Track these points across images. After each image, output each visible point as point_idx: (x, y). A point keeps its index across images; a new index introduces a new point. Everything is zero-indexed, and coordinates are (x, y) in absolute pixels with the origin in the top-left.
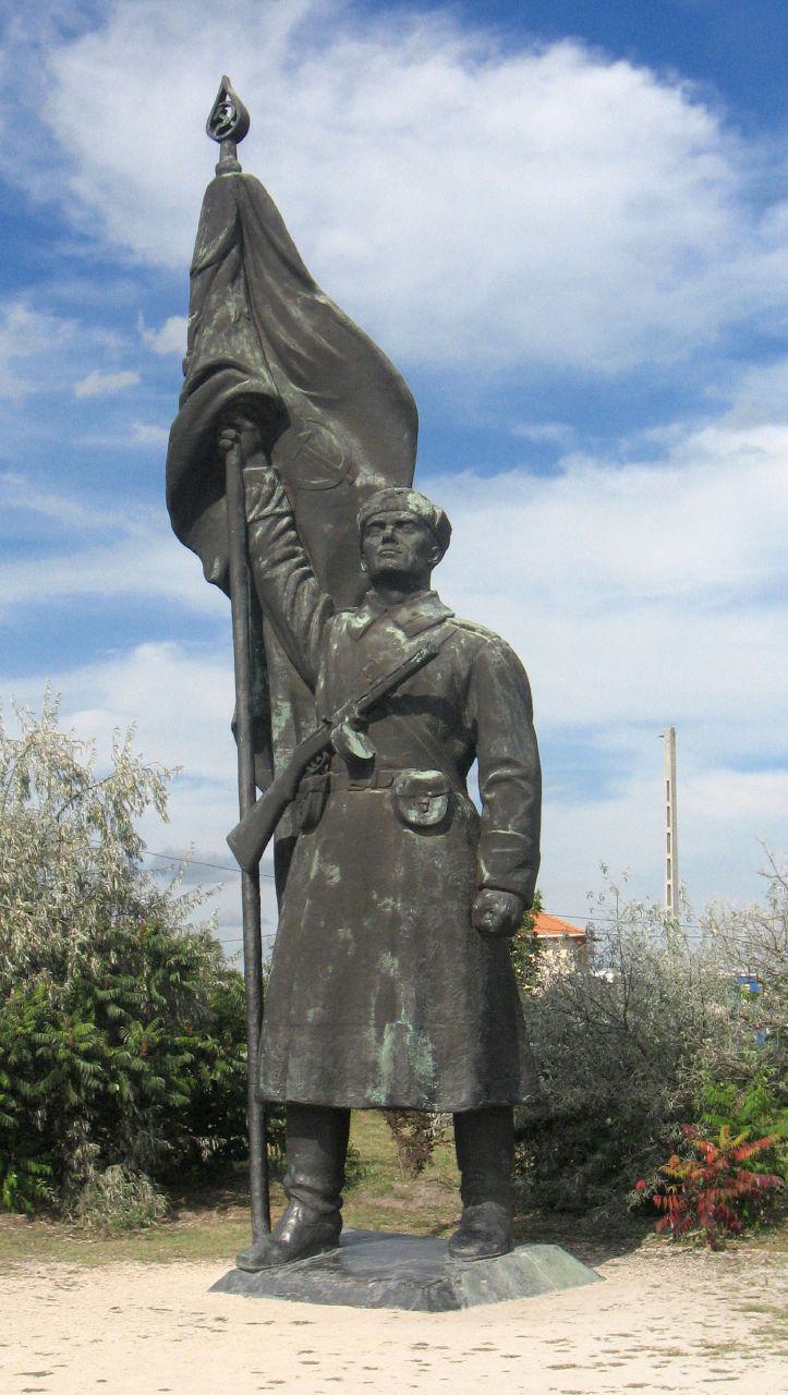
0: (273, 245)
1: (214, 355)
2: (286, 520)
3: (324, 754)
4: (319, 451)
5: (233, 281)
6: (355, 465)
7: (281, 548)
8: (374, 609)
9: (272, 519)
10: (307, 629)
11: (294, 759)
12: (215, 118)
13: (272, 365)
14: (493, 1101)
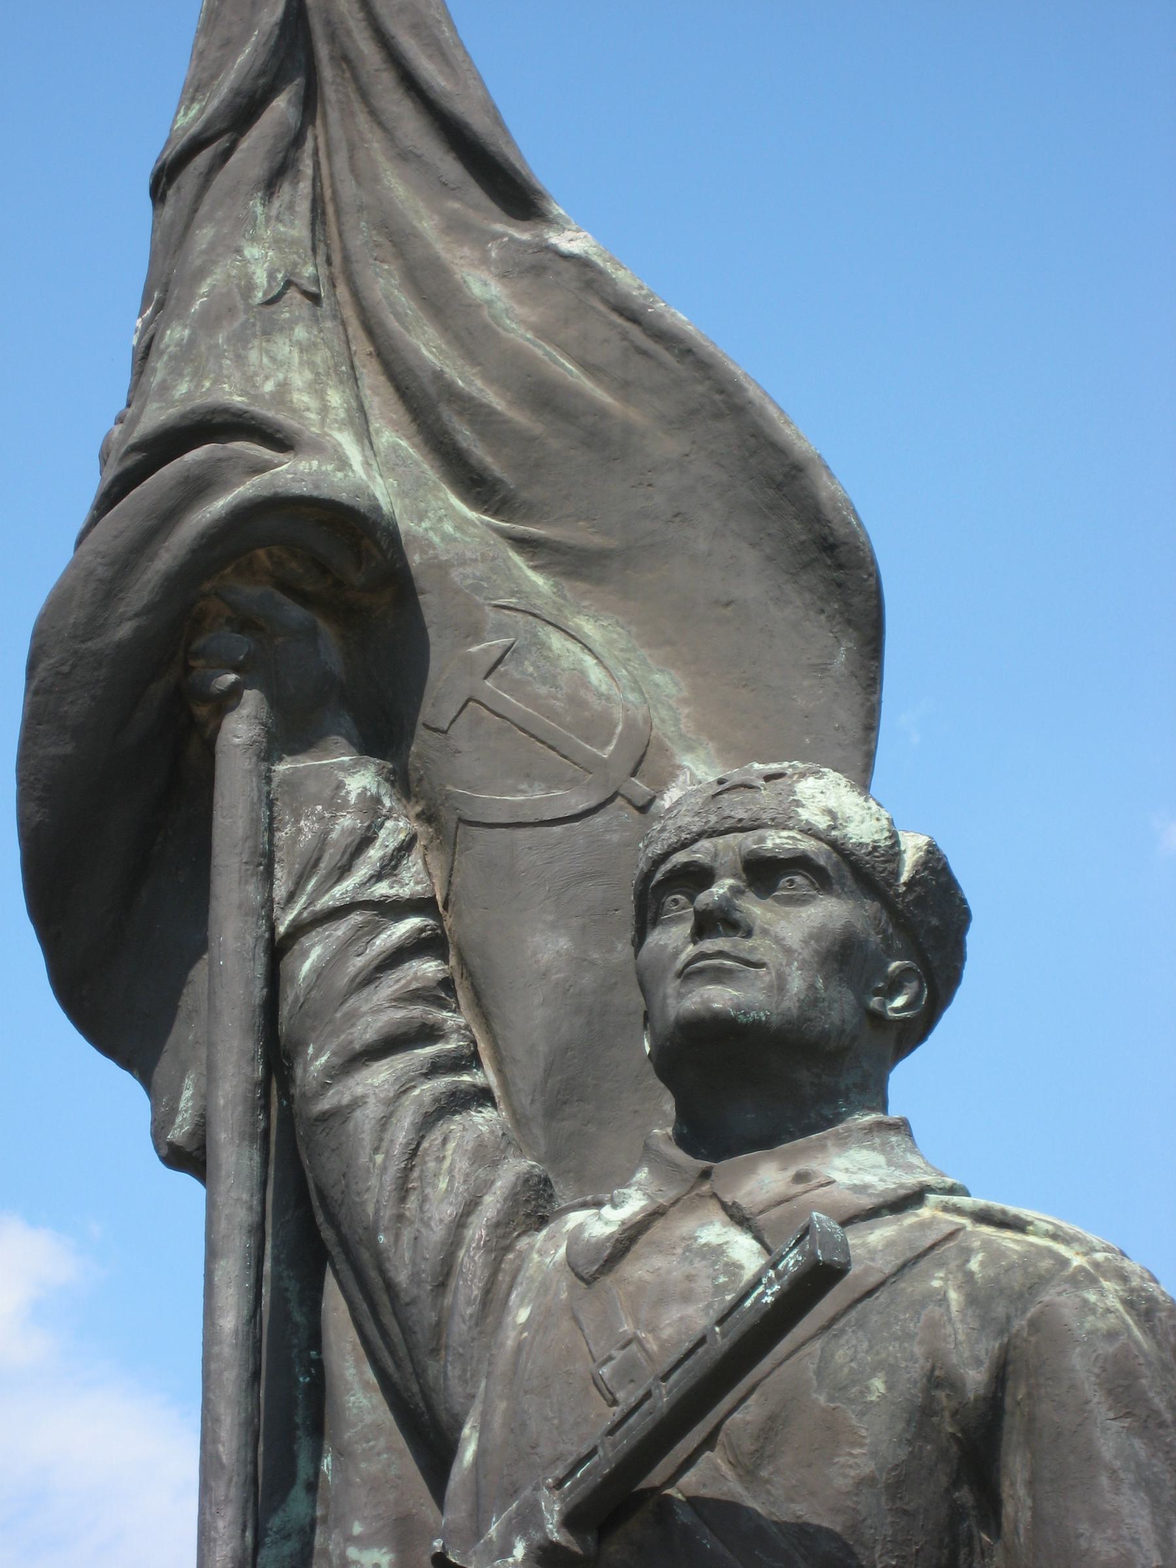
0: (410, 82)
1: (189, 395)
4: (533, 700)
6: (663, 750)
7: (377, 1010)
8: (664, 1169)
9: (356, 918)
13: (386, 437)
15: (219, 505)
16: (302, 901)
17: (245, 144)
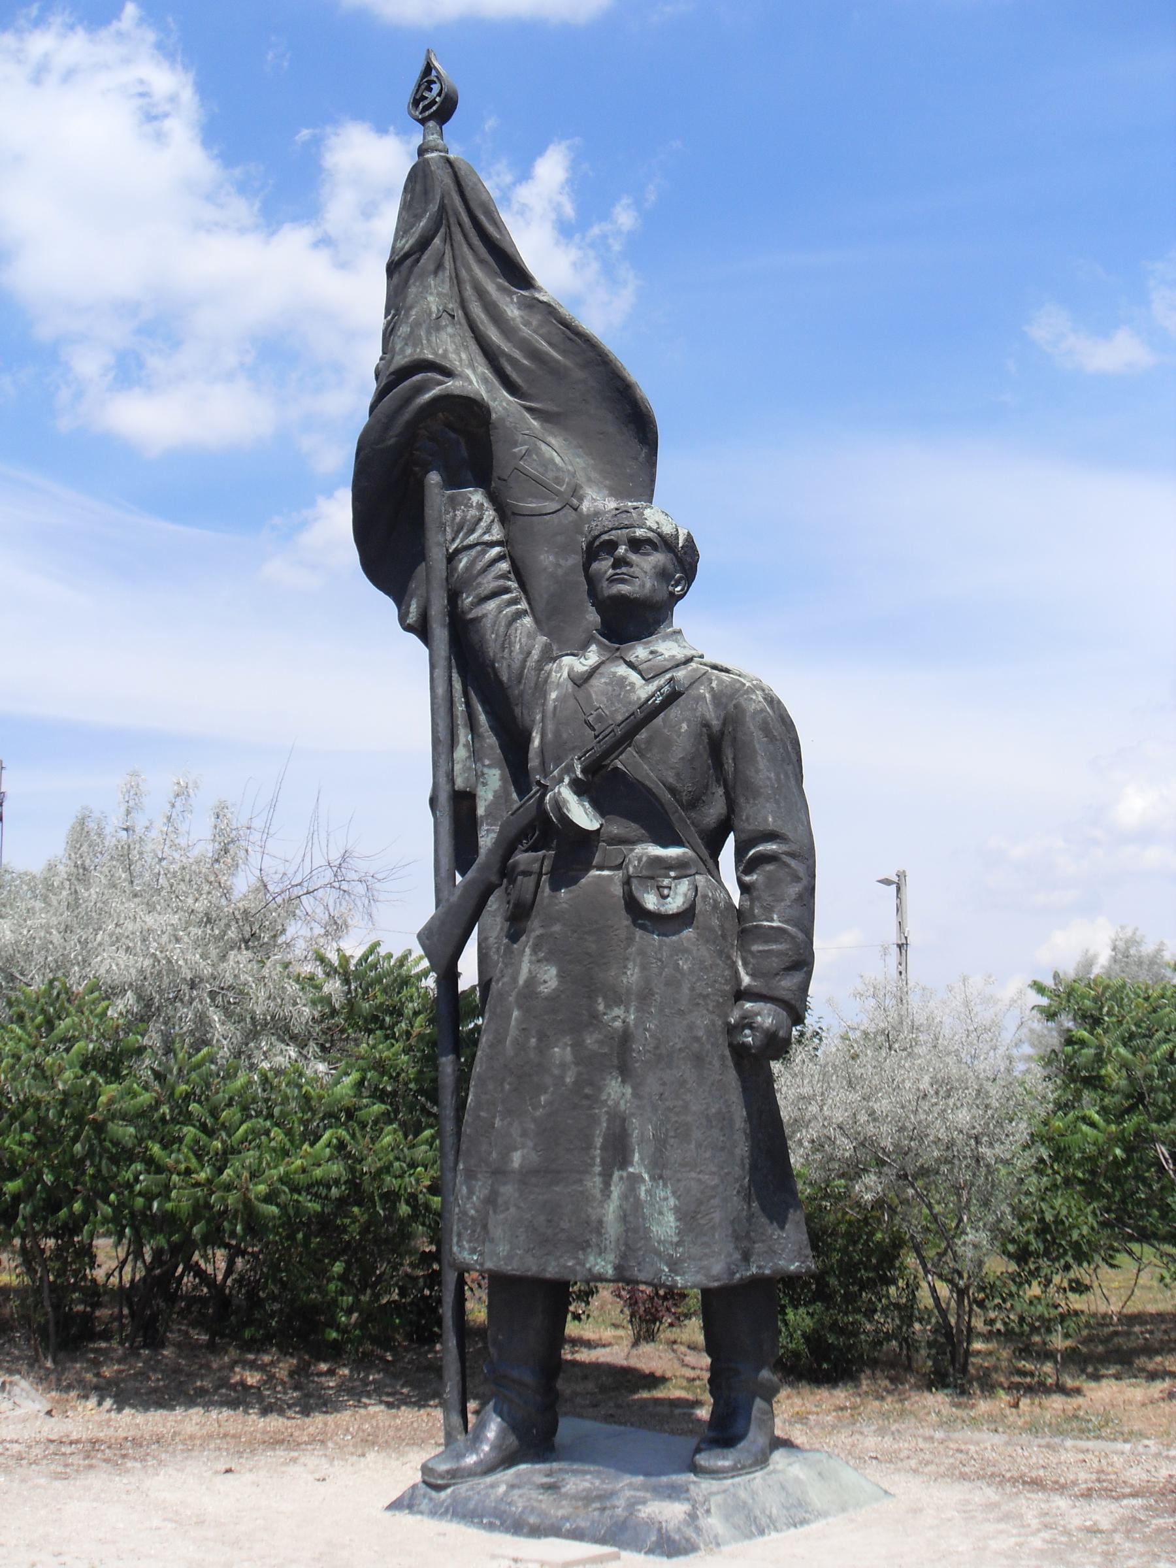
1: (411, 354)
2: (496, 551)
5: (436, 273)
9: (479, 548)
11: (497, 843)
15: (427, 396)
16: (458, 541)
17: (425, 257)
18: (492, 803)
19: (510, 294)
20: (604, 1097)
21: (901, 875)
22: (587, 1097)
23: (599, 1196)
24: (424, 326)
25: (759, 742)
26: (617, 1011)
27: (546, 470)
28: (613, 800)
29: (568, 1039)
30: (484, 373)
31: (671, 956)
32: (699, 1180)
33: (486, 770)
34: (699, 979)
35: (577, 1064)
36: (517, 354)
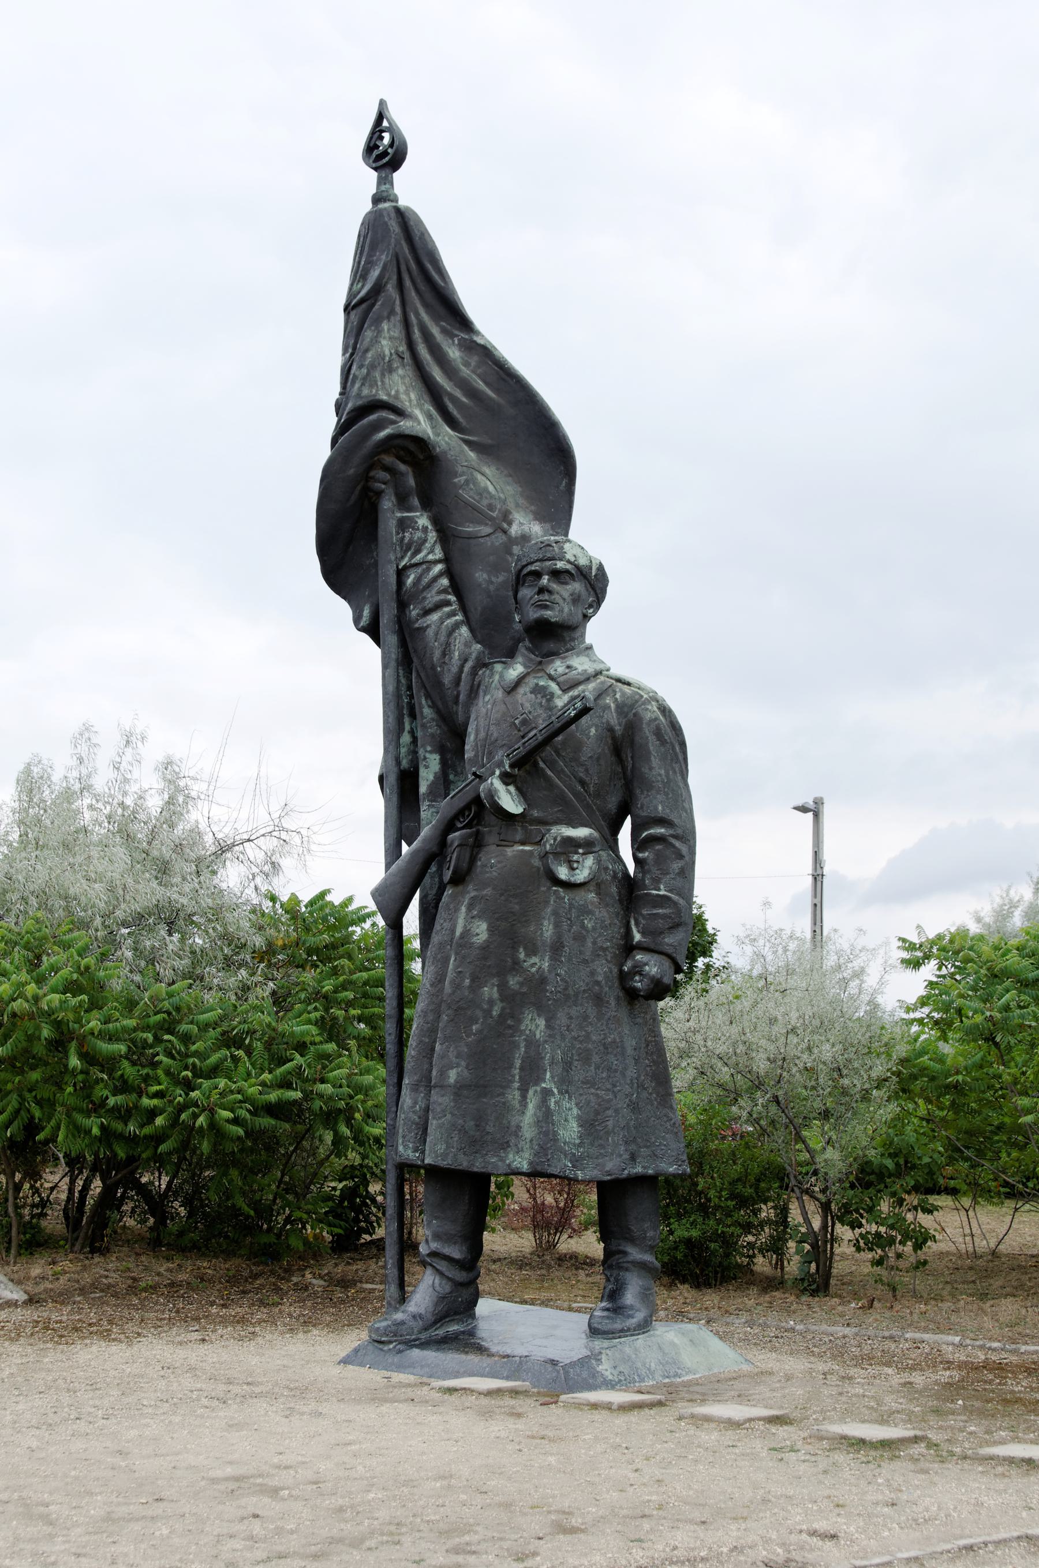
3: (479, 812)
9: (424, 566)
10: (457, 681)
12: (372, 145)
14: (639, 1170)
15: (383, 434)
16: (406, 559)
18: (433, 783)
19: (452, 336)
20: (523, 1028)
21: (819, 802)
22: (510, 1027)
23: (517, 1106)
24: (379, 369)
25: (652, 744)
26: (535, 960)
27: (481, 498)
28: (534, 773)
29: (495, 981)
30: (429, 410)
31: (579, 916)
32: (597, 1095)
33: (428, 755)
34: (600, 935)
35: (502, 1001)
36: (458, 393)
